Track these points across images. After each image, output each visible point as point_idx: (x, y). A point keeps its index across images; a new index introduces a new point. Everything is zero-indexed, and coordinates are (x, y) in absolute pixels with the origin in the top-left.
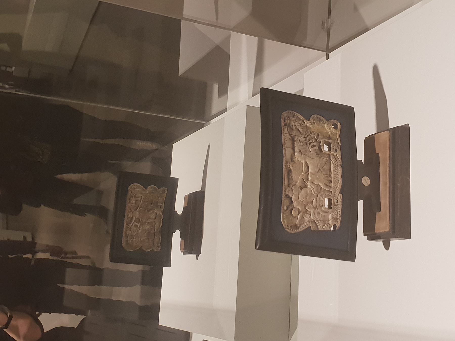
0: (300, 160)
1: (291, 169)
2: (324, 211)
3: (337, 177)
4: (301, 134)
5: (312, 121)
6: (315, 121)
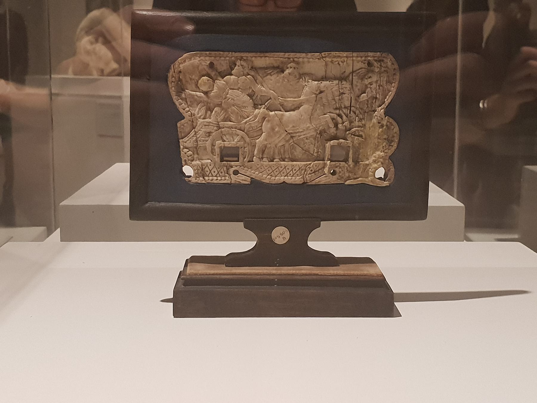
0: (304, 91)
1: (285, 72)
2: (215, 146)
3: (282, 173)
4: (357, 98)
5: (385, 123)
6: (385, 127)
